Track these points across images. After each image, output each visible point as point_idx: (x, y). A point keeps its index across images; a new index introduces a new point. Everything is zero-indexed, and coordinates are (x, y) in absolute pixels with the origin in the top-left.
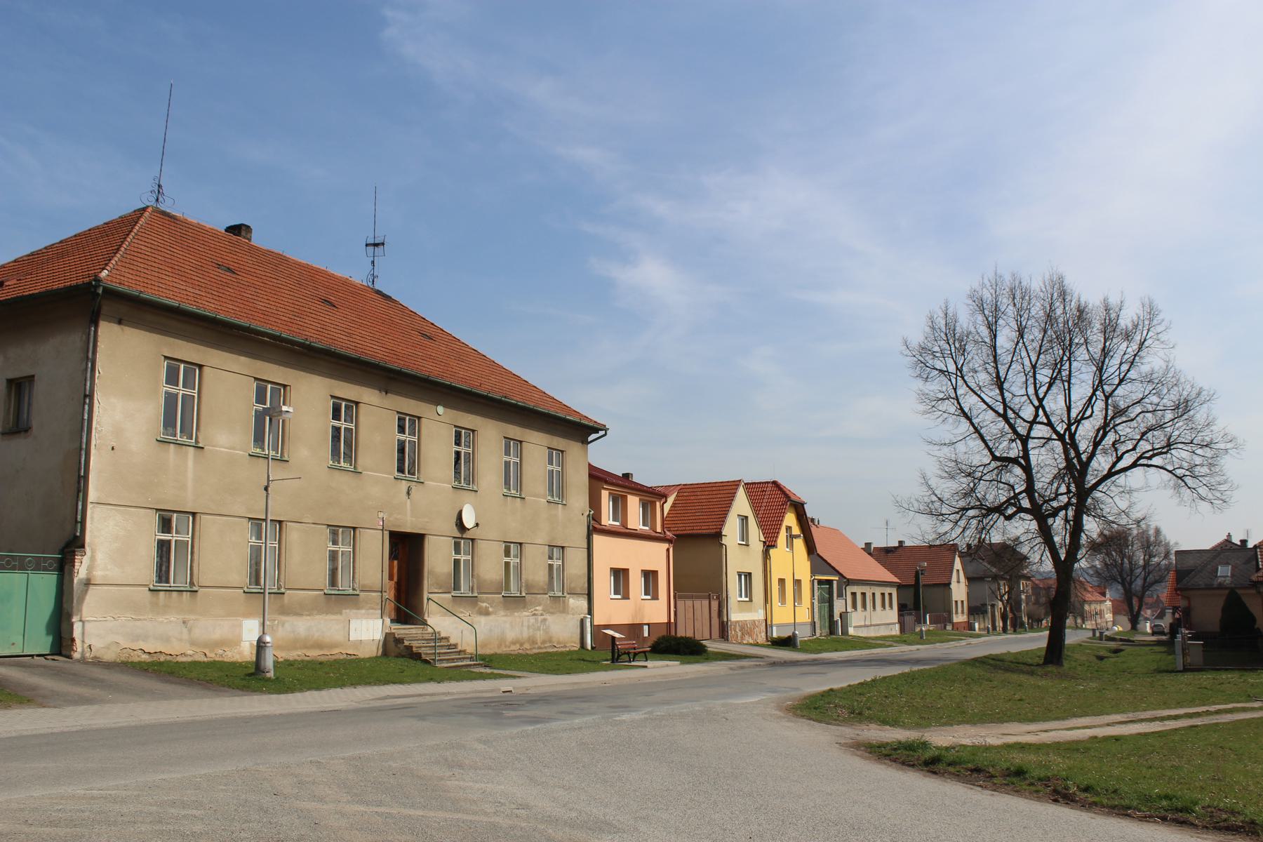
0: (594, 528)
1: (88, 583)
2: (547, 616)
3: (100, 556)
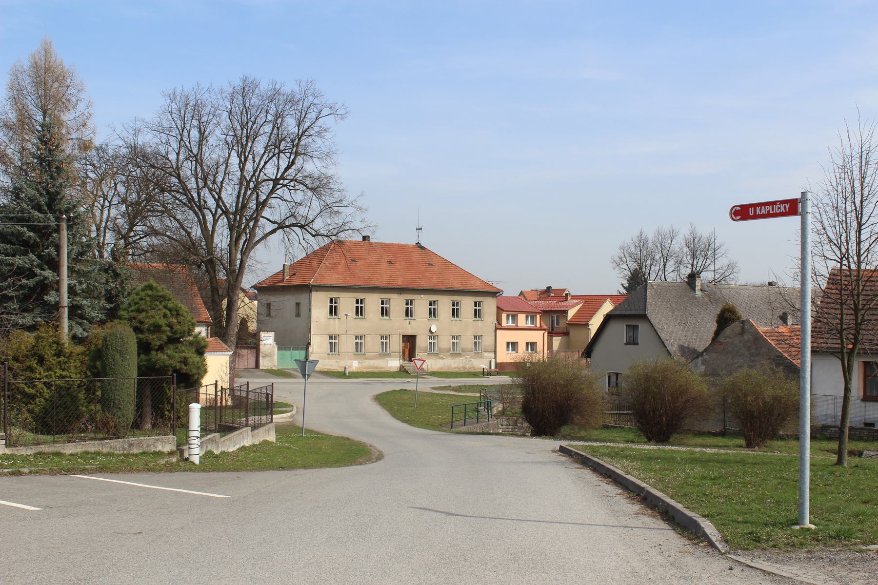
0: (499, 326)
1: (311, 353)
2: (472, 359)
3: (314, 347)
